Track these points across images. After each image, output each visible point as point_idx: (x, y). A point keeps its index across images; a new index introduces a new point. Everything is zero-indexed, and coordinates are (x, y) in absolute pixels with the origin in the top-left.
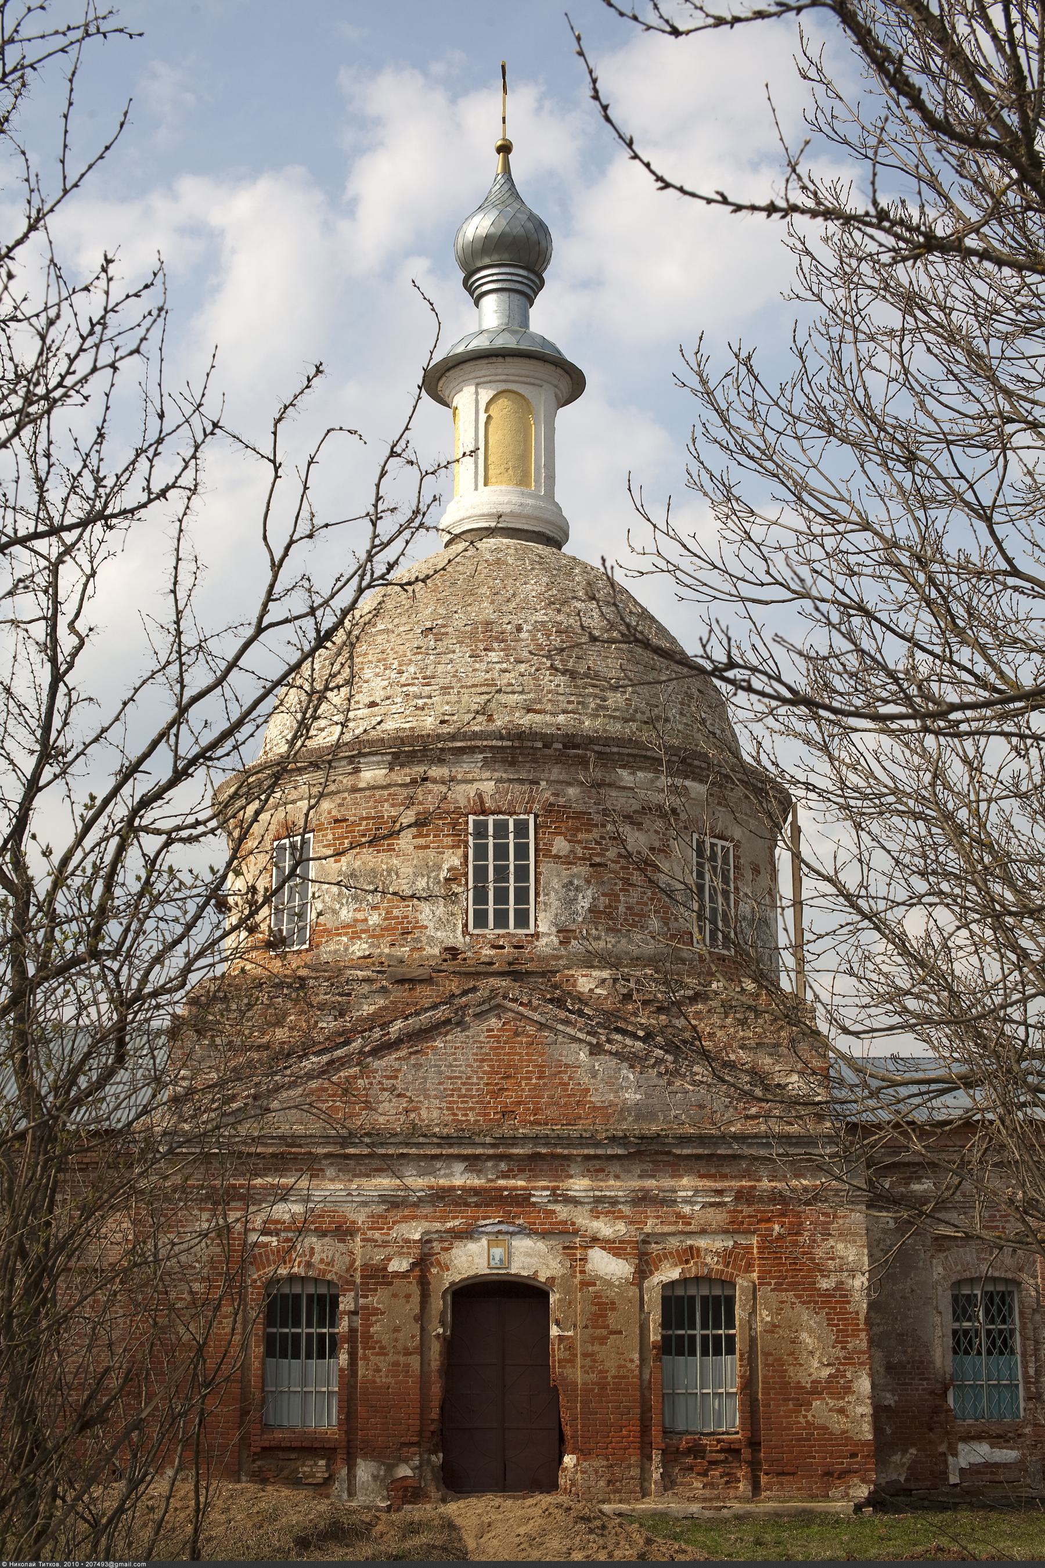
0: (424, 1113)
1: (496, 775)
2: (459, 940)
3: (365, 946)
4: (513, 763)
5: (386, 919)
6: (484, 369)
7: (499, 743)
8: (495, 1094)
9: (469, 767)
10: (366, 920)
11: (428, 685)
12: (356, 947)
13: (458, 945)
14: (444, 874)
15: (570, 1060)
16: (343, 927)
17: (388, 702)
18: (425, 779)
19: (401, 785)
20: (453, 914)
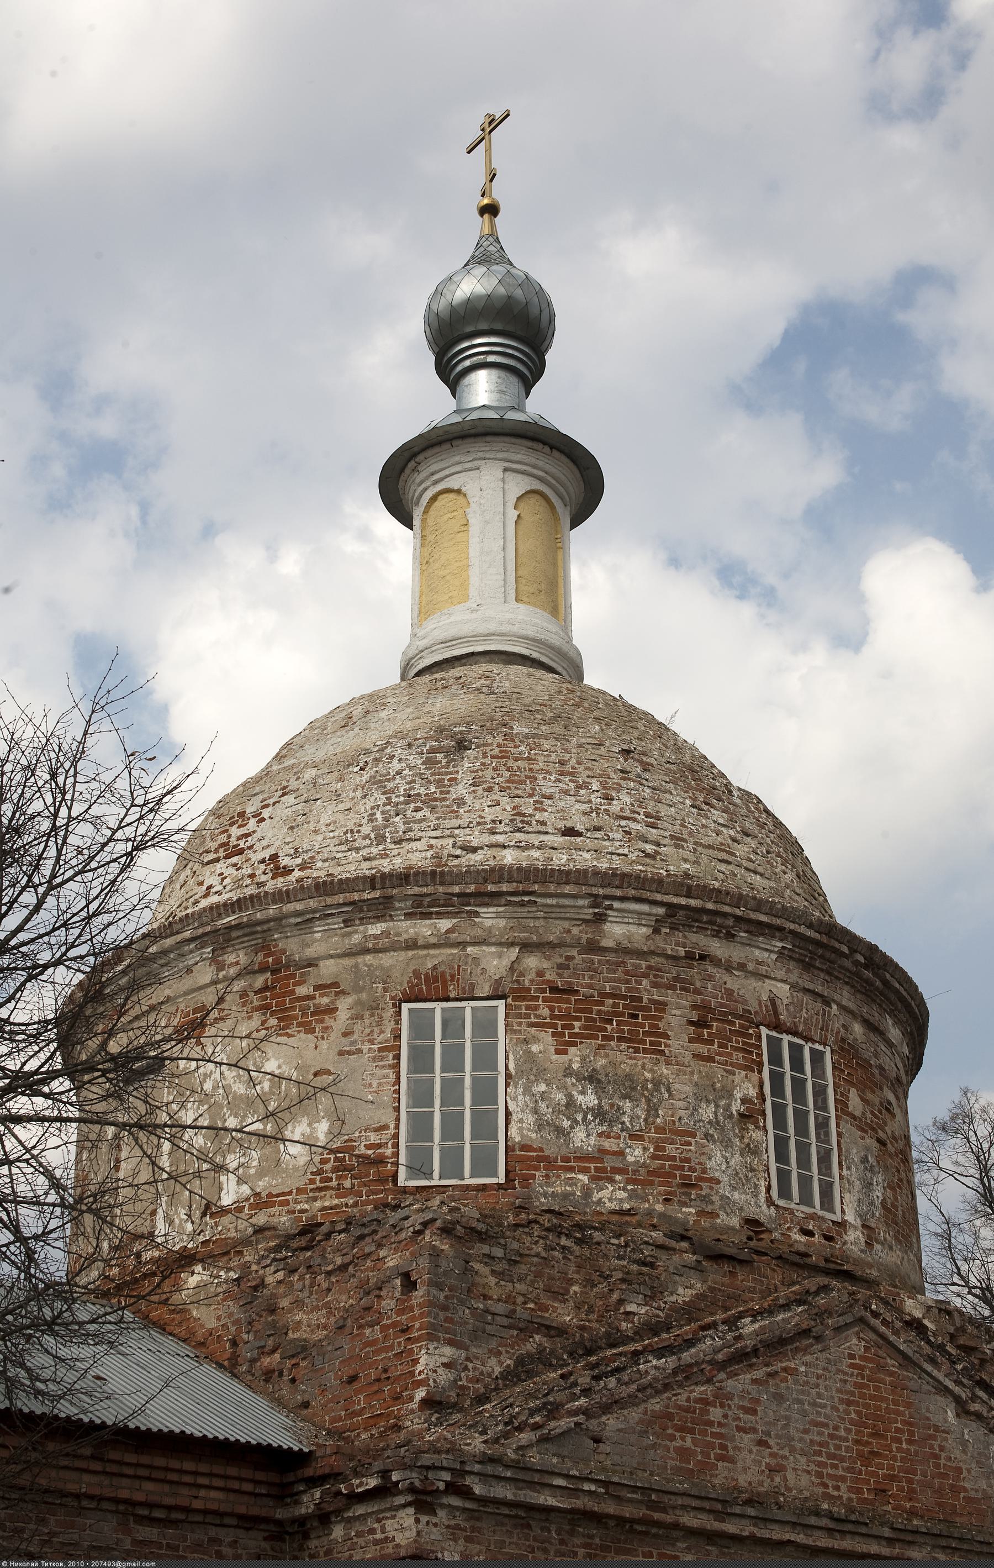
0: (790, 1475)
1: (794, 977)
2: (765, 1213)
3: (623, 1195)
4: (807, 966)
5: (654, 1157)
6: (521, 454)
7: (809, 933)
8: (867, 1459)
9: (763, 953)
10: (621, 1153)
11: (653, 826)
12: (605, 1194)
13: (763, 1219)
14: (736, 1107)
15: (936, 1419)
16: (578, 1159)
17: (598, 835)
18: (703, 958)
19: (668, 957)
20: (752, 1170)
